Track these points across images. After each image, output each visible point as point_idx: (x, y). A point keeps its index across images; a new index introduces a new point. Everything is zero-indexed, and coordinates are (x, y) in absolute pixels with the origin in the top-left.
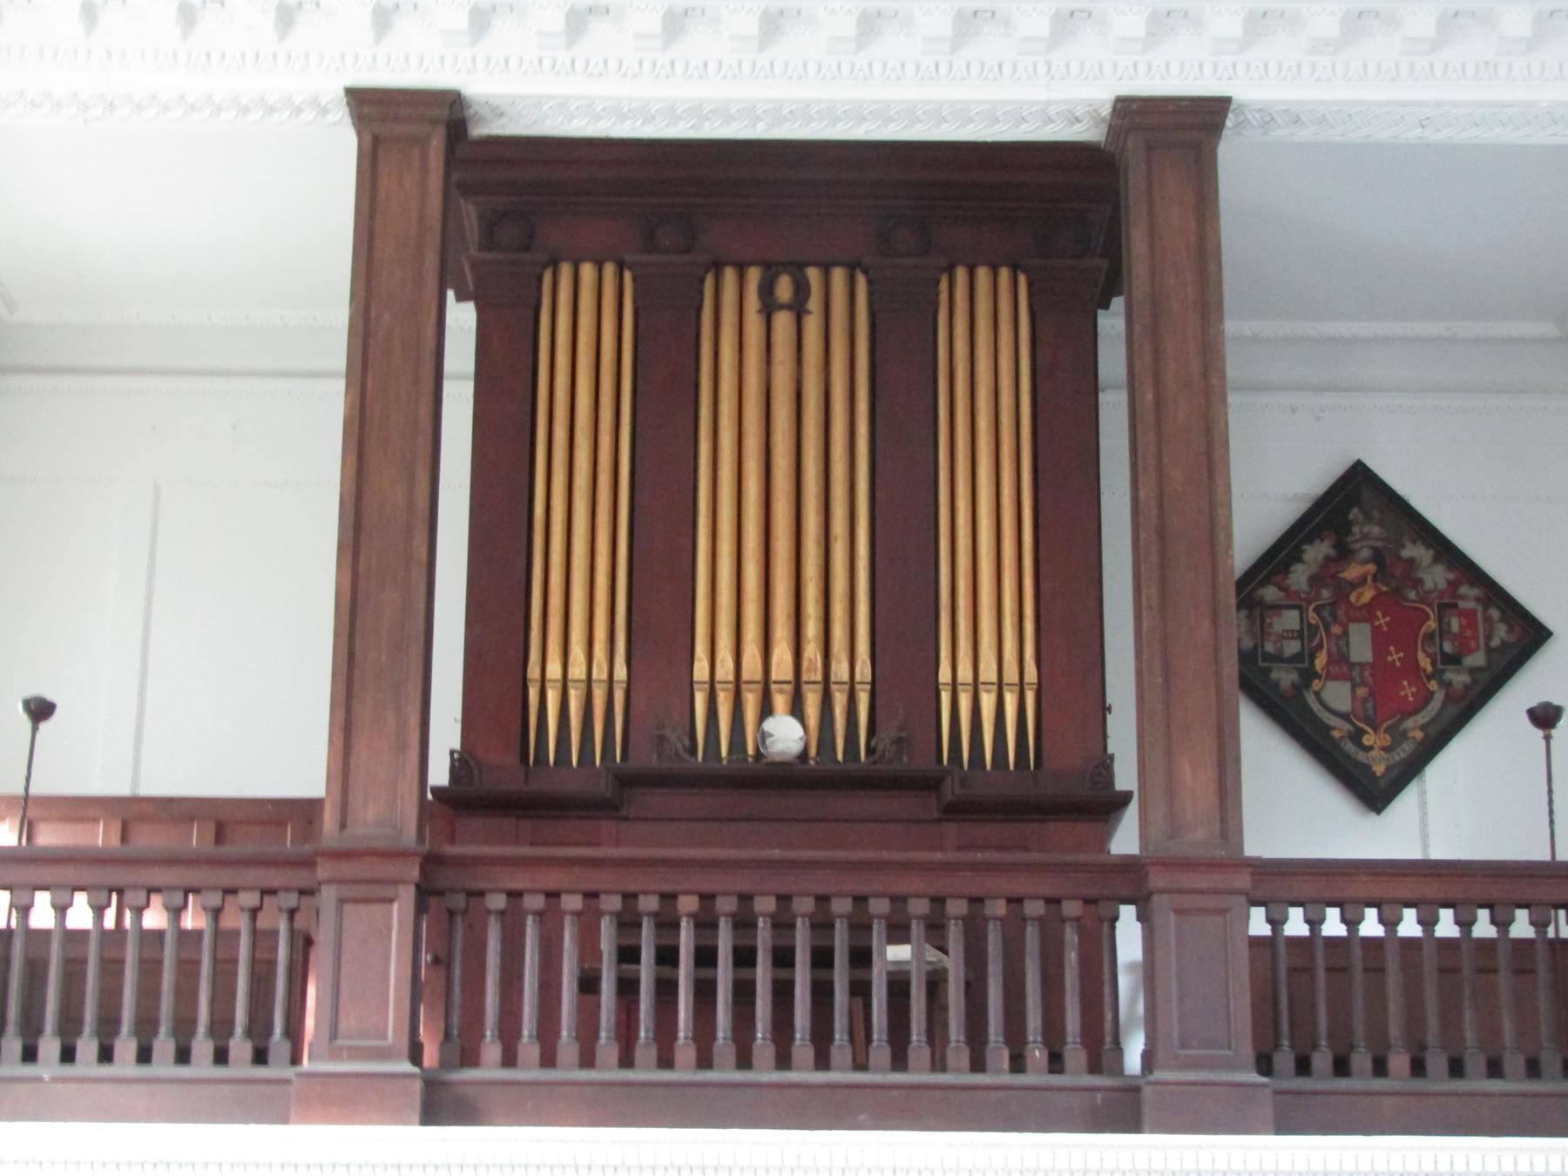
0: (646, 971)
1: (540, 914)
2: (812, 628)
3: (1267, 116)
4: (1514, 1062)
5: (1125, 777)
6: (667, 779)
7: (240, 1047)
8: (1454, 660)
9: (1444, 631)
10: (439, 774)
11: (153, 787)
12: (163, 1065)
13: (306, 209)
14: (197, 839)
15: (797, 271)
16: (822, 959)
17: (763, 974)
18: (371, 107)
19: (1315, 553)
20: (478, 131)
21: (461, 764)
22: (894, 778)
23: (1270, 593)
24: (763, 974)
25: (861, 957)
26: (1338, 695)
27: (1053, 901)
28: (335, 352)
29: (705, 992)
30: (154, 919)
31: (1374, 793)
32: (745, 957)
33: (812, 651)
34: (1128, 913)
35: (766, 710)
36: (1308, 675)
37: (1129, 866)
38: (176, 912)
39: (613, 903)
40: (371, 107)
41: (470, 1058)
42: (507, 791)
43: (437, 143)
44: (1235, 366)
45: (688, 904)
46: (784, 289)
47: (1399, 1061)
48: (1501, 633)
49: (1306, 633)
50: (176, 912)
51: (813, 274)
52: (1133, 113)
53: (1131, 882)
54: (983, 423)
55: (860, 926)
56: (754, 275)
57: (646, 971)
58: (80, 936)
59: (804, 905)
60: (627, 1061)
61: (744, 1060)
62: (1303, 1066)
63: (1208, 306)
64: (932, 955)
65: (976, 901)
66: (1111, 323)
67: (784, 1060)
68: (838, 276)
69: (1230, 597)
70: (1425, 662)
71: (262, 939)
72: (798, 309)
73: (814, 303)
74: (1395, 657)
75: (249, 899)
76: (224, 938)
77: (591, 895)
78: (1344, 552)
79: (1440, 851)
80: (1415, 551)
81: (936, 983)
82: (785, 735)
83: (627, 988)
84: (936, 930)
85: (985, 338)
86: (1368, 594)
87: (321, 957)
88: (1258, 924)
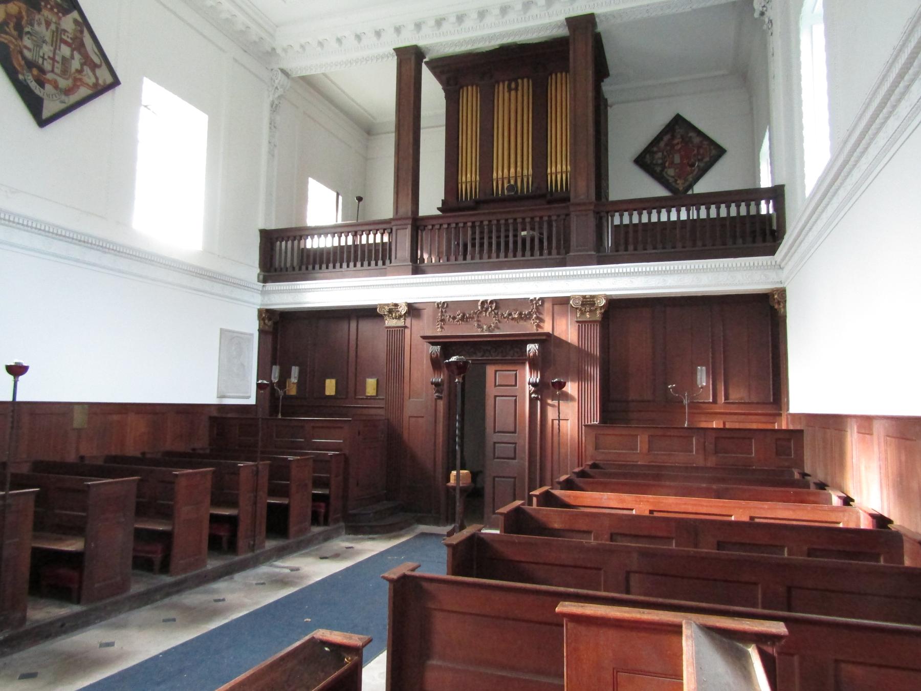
3: (605, 15)
9: (698, 153)
15: (516, 80)
19: (666, 138)
25: (515, 236)
26: (671, 172)
33: (519, 169)
36: (664, 167)
46: (513, 85)
48: (714, 152)
49: (664, 158)
51: (520, 81)
52: (574, 23)
54: (559, 110)
55: (515, 230)
56: (506, 83)
64: (531, 232)
68: (525, 80)
72: (516, 89)
73: (520, 88)
78: (673, 137)
80: (692, 134)
81: (532, 240)
84: (533, 229)
85: (561, 93)
86: (679, 146)
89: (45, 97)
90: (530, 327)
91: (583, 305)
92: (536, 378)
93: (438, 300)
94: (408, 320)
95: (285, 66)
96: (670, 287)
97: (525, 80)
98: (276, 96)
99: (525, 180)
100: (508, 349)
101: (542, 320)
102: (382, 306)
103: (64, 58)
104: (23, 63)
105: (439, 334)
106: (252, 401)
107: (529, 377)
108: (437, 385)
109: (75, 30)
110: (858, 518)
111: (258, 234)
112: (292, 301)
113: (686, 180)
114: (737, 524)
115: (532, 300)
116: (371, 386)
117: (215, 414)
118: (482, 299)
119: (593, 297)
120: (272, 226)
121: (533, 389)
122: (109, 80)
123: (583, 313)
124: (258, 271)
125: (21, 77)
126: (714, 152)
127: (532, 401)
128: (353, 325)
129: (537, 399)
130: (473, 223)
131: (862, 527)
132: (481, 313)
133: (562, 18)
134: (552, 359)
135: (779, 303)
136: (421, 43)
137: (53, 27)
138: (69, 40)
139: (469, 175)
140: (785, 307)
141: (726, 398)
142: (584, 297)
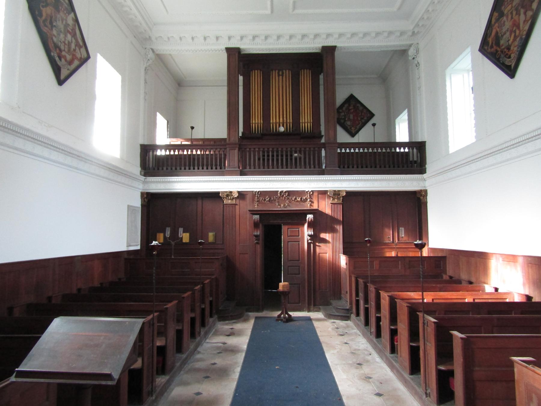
0: (266, 157)
1: (253, 151)
2: (285, 116)
3: (341, 47)
4: (369, 166)
5: (323, 133)
6: (267, 135)
7: (218, 167)
8: (362, 119)
10: (240, 135)
11: (207, 137)
12: (210, 169)
13: (221, 64)
14: (212, 143)
16: (287, 156)
17: (280, 158)
19: (346, 105)
20: (242, 53)
21: (243, 133)
22: (294, 134)
23: (341, 111)
24: (280, 158)
25: (291, 156)
26: (349, 123)
27: (314, 148)
28: (226, 83)
29: (273, 160)
30: (207, 153)
31: (353, 135)
32: (277, 156)
33: (285, 119)
34: (323, 149)
35: (279, 126)
36: (345, 121)
37: (324, 144)
38: (210, 152)
39: (262, 149)
40: (228, 50)
41: (246, 168)
42: (249, 136)
43: (237, 54)
44: (337, 83)
45: (271, 149)
46: (281, 73)
47: (355, 166)
49: (345, 116)
50: (210, 152)
51: (284, 71)
52: (324, 48)
53: (324, 145)
55: (291, 152)
56: (277, 71)
57: (266, 157)
58: (199, 155)
59: (284, 149)
60: (264, 168)
61: (278, 168)
62: (344, 167)
63: (334, 73)
64: (300, 155)
65: (305, 148)
66: (321, 77)
67: (282, 168)
69: (336, 111)
70: (359, 119)
71: (220, 155)
72: (283, 76)
73: (284, 75)
74: (356, 118)
75: (219, 150)
76: (216, 155)
77: (259, 149)
78: (349, 105)
79: (360, 141)
80: (359, 105)
81: (300, 158)
82: (282, 129)
83: (264, 160)
84: (300, 152)
87: (227, 157)
88: (339, 151)
89: (61, 66)
90: (307, 206)
91: (334, 195)
92: (311, 232)
93: (255, 190)
94: (238, 201)
95: (154, 47)
97: (287, 71)
98: (148, 64)
99: (288, 125)
100: (298, 218)
101: (312, 202)
102: (223, 192)
103: (69, 42)
104: (53, 45)
105: (256, 209)
106: (138, 248)
107: (307, 232)
108: (256, 236)
109: (73, 25)
110: (514, 297)
111: (139, 147)
112: (164, 188)
113: (356, 128)
114: (468, 303)
115: (307, 192)
116: (211, 236)
117: (126, 256)
118: (280, 190)
119: (339, 191)
120: (146, 143)
121: (309, 238)
122: (84, 55)
123: (334, 199)
124: (140, 169)
125: (52, 54)
127: (309, 244)
128: (200, 202)
129: (311, 243)
130: (273, 149)
131: (515, 301)
132: (280, 198)
133: (320, 46)
134: (321, 223)
135: (424, 197)
137: (64, 22)
138: (70, 31)
139: (256, 119)
140: (426, 198)
141: (398, 240)
142: (335, 191)
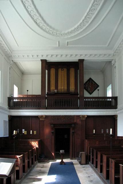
3: (86, 60)
5: (79, 93)
13: (38, 66)
15: (63, 68)
18: (42, 60)
21: (47, 93)
26: (89, 89)
31: (91, 94)
33: (64, 87)
40: (42, 60)
43: (45, 62)
46: (62, 69)
48: (97, 86)
52: (79, 60)
53: (79, 98)
63: (83, 70)
72: (63, 70)
85: (72, 71)
88: (85, 100)
96: (98, 114)
126: (97, 86)
133: (78, 59)
136: (47, 59)
